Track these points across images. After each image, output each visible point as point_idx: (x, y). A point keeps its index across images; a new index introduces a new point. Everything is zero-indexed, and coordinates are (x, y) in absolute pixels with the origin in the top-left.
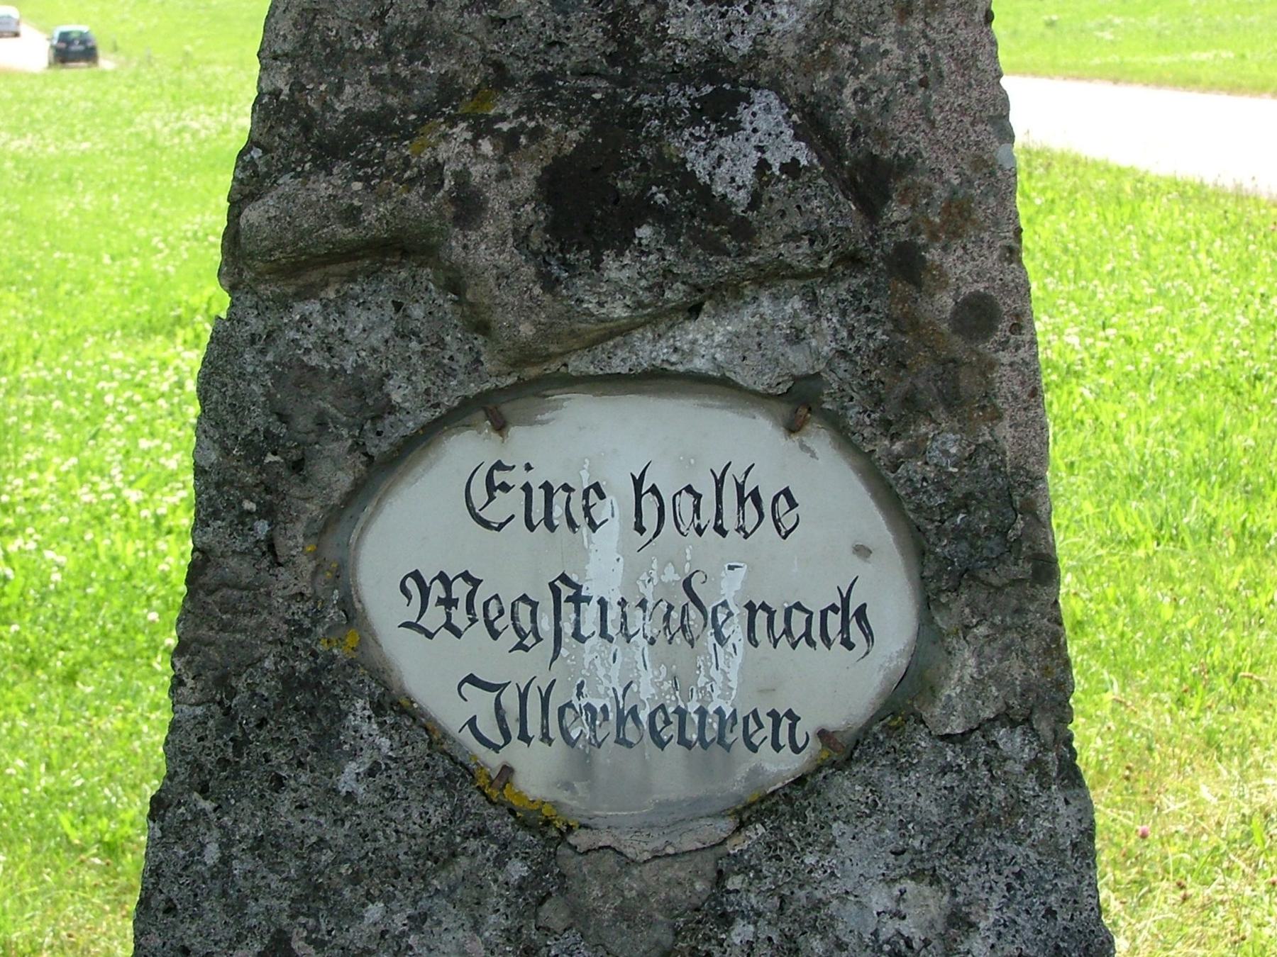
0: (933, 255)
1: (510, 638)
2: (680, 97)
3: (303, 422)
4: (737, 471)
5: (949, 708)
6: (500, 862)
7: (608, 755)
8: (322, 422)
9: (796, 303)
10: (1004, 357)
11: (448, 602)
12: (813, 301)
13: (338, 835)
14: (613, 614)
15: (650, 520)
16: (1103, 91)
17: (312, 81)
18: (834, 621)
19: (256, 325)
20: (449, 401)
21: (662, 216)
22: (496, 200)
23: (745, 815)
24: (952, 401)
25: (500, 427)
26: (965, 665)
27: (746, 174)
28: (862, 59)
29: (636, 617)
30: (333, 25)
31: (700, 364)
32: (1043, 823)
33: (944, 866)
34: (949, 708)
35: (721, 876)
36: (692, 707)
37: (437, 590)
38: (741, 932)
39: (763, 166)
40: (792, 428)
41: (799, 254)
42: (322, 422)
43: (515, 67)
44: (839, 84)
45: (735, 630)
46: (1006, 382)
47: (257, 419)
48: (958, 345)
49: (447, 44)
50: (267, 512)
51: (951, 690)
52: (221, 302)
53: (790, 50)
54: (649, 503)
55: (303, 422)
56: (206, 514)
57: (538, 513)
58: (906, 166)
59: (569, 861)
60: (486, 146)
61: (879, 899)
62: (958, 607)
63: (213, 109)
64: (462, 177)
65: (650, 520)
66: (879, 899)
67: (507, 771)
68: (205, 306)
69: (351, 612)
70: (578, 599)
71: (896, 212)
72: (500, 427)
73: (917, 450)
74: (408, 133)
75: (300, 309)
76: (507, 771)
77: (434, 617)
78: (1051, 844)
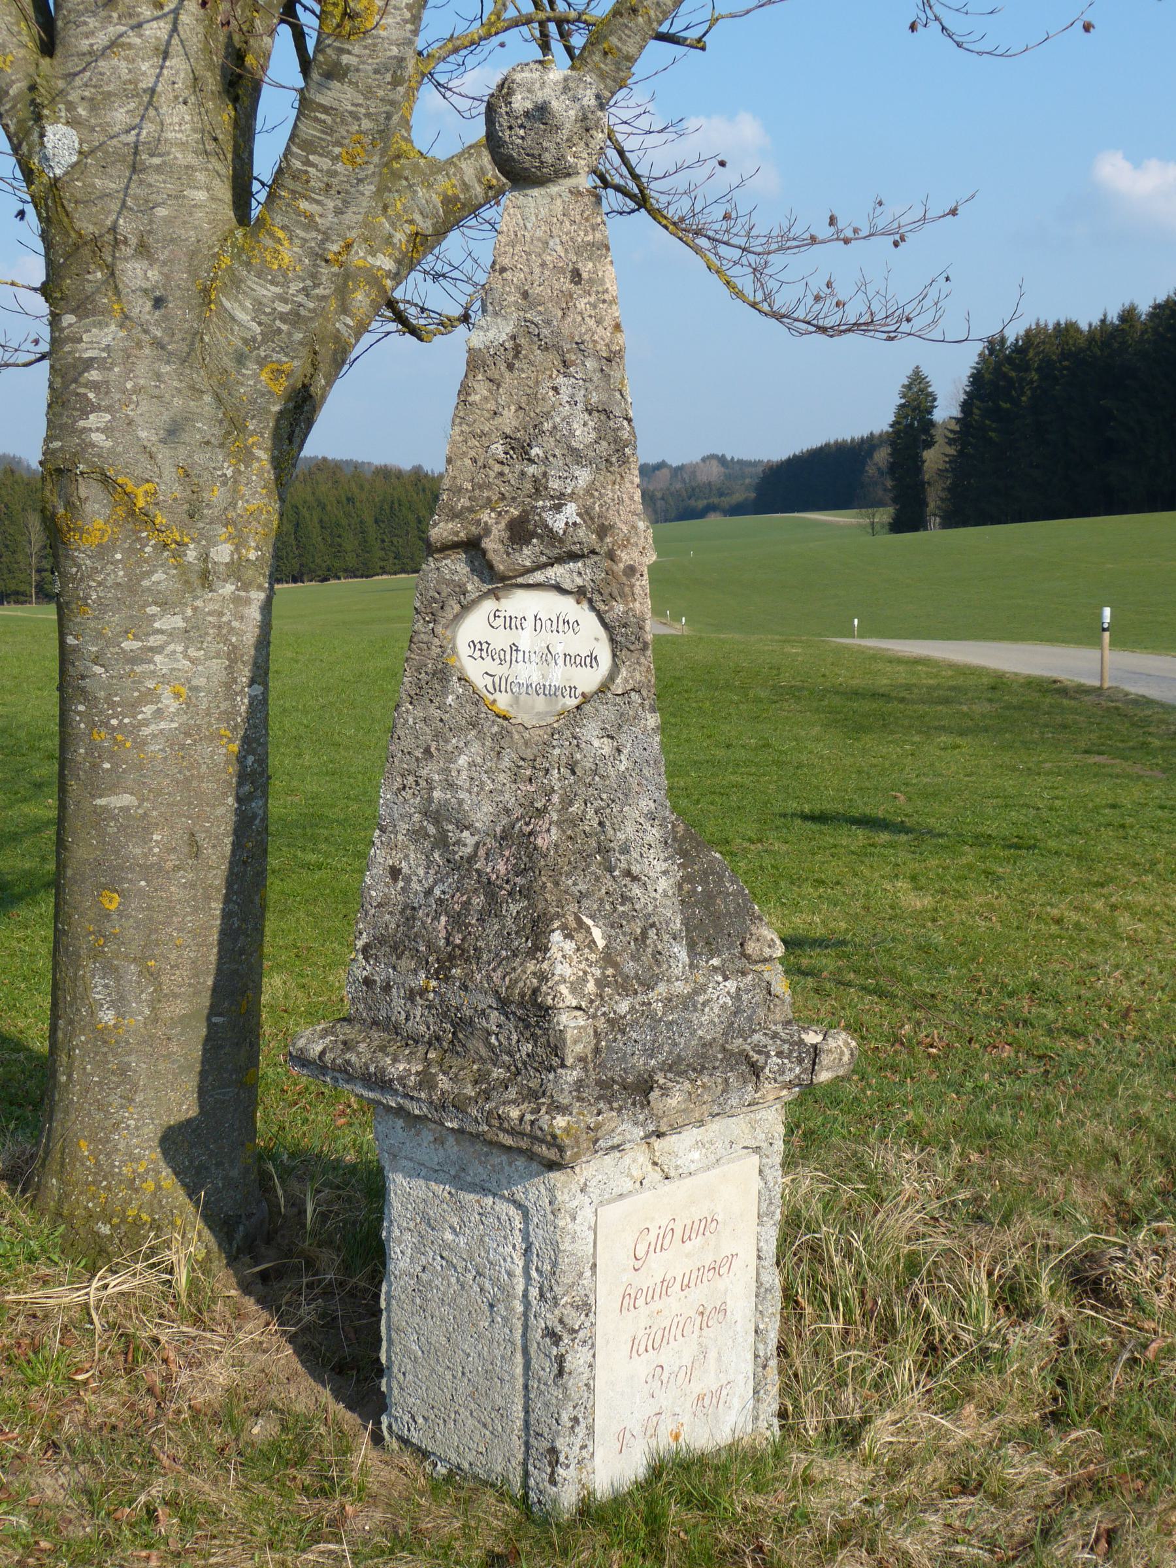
0: (618, 552)
4: (563, 614)
5: (618, 686)
7: (523, 697)
10: (638, 583)
11: (481, 650)
14: (527, 655)
15: (538, 628)
18: (588, 660)
21: (540, 537)
24: (623, 595)
26: (624, 672)
27: (563, 525)
29: (533, 655)
32: (643, 722)
34: (618, 686)
36: (547, 684)
37: (478, 646)
39: (567, 524)
43: (507, 494)
44: (594, 503)
45: (560, 661)
48: (624, 580)
53: (581, 492)
54: (538, 622)
57: (507, 625)
58: (612, 527)
60: (493, 515)
64: (486, 523)
65: (538, 628)
67: (494, 701)
70: (517, 650)
71: (608, 540)
72: (498, 599)
74: (475, 512)
75: (445, 562)
76: (494, 701)
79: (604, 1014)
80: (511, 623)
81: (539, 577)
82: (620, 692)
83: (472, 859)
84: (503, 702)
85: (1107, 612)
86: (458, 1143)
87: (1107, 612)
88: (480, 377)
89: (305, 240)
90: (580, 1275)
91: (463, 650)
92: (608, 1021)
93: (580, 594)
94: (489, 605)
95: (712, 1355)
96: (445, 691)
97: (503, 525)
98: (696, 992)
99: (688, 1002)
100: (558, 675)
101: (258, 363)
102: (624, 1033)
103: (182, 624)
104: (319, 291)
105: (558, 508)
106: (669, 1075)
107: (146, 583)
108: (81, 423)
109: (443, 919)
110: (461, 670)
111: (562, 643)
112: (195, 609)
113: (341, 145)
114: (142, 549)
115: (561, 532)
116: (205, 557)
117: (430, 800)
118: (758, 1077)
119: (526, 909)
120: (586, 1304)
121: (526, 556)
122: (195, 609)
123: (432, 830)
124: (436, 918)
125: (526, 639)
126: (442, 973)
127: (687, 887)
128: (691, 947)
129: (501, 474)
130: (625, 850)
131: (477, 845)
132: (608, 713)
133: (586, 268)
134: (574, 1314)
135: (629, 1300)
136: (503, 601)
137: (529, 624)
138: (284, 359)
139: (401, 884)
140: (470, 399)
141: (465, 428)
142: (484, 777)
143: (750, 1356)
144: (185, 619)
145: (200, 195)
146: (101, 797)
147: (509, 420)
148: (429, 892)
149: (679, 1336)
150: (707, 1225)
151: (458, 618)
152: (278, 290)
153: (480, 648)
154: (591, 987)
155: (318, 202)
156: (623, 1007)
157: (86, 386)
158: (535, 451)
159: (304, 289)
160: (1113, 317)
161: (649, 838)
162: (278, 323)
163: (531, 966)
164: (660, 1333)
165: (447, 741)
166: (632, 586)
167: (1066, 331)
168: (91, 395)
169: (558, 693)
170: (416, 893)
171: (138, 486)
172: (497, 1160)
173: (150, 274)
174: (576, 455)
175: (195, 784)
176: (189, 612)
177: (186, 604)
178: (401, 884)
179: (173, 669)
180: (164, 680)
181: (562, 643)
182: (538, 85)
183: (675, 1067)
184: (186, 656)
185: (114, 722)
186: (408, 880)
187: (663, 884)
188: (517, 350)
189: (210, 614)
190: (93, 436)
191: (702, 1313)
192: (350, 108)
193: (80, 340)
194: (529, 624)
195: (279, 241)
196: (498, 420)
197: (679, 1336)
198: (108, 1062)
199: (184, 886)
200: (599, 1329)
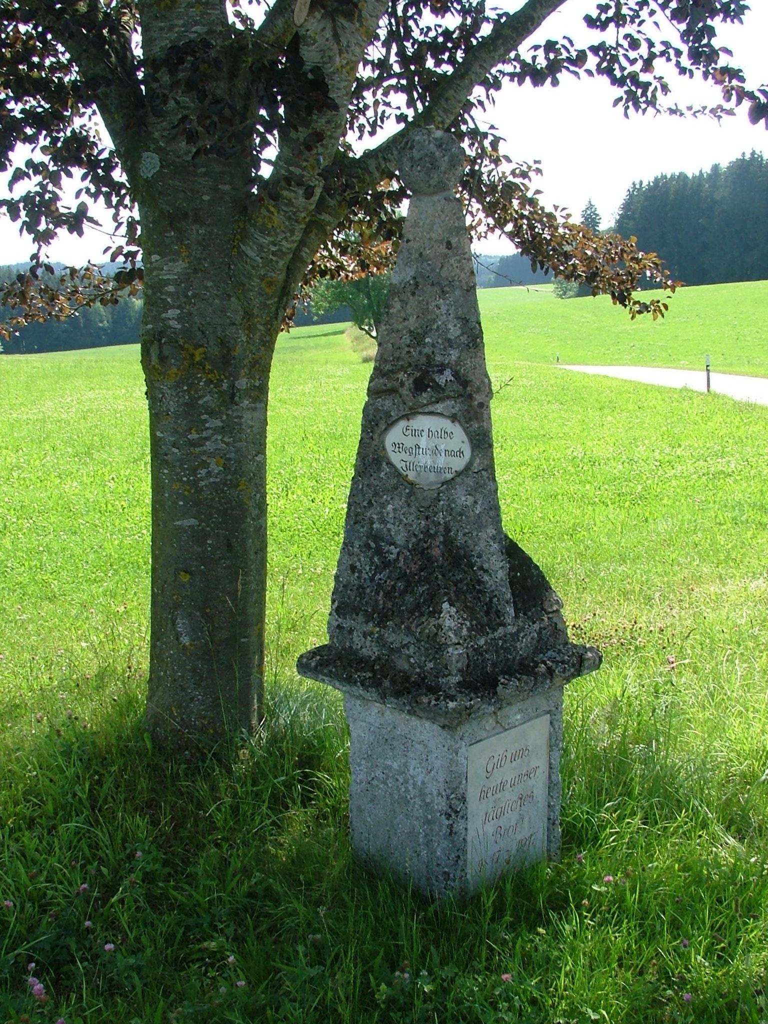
2: (436, 369)
3: (378, 417)
7: (423, 473)
8: (381, 418)
13: (380, 484)
16: (667, 370)
17: (206, 548)
19: (371, 402)
21: (431, 387)
22: (406, 384)
23: (443, 484)
24: (477, 419)
26: (478, 461)
28: (465, 365)
30: (386, 356)
33: (473, 493)
38: (442, 502)
40: (453, 422)
41: (452, 394)
42: (381, 418)
45: (443, 454)
46: (485, 416)
47: (371, 417)
49: (403, 359)
50: (372, 432)
51: (475, 465)
52: (367, 399)
55: (378, 417)
56: (363, 431)
58: (471, 381)
59: (415, 490)
61: (463, 499)
62: (477, 452)
63: (709, 822)
66: (463, 499)
69: (384, 448)
71: (469, 388)
73: (471, 426)
74: (396, 373)
77: (397, 450)
78: (490, 491)
79: (472, 646)
81: (431, 408)
83: (397, 560)
84: (411, 476)
86: (392, 714)
88: (396, 299)
89: (287, 212)
90: (460, 783)
91: (389, 447)
93: (454, 418)
94: (403, 424)
95: (526, 820)
96: (379, 470)
97: (411, 381)
98: (519, 631)
99: (515, 636)
100: (441, 461)
101: (260, 278)
102: (482, 655)
103: (220, 424)
105: (441, 372)
106: (506, 677)
107: (200, 402)
108: (164, 315)
109: (381, 593)
110: (388, 459)
112: (228, 415)
113: (307, 161)
114: (198, 384)
116: (232, 386)
117: (372, 529)
118: (552, 675)
119: (428, 589)
120: (463, 797)
121: (424, 397)
122: (228, 415)
123: (373, 545)
124: (378, 593)
125: (423, 442)
127: (512, 574)
128: (517, 611)
129: (409, 352)
130: (480, 556)
131: (398, 553)
132: (470, 482)
133: (454, 241)
134: (457, 803)
137: (425, 434)
139: (357, 574)
140: (391, 311)
141: (388, 327)
142: (402, 517)
143: (546, 819)
144: (222, 421)
145: (227, 188)
147: (412, 323)
148: (372, 579)
149: (509, 811)
150: (523, 752)
152: (271, 239)
153: (398, 446)
154: (465, 632)
156: (482, 642)
157: (166, 294)
159: (285, 238)
160: (707, 169)
161: (492, 550)
162: (271, 256)
163: (433, 622)
165: (381, 497)
166: (482, 413)
167: (682, 177)
168: (169, 300)
170: (365, 579)
171: (196, 349)
172: (414, 723)
173: (200, 231)
175: (229, 512)
176: (224, 417)
177: (223, 413)
178: (357, 574)
179: (217, 449)
180: (211, 455)
183: (509, 672)
185: (185, 479)
186: (360, 572)
187: (501, 574)
188: (417, 285)
193: (162, 269)
194: (425, 434)
195: (272, 213)
196: (406, 323)
197: (509, 811)
199: (225, 568)
200: (469, 811)
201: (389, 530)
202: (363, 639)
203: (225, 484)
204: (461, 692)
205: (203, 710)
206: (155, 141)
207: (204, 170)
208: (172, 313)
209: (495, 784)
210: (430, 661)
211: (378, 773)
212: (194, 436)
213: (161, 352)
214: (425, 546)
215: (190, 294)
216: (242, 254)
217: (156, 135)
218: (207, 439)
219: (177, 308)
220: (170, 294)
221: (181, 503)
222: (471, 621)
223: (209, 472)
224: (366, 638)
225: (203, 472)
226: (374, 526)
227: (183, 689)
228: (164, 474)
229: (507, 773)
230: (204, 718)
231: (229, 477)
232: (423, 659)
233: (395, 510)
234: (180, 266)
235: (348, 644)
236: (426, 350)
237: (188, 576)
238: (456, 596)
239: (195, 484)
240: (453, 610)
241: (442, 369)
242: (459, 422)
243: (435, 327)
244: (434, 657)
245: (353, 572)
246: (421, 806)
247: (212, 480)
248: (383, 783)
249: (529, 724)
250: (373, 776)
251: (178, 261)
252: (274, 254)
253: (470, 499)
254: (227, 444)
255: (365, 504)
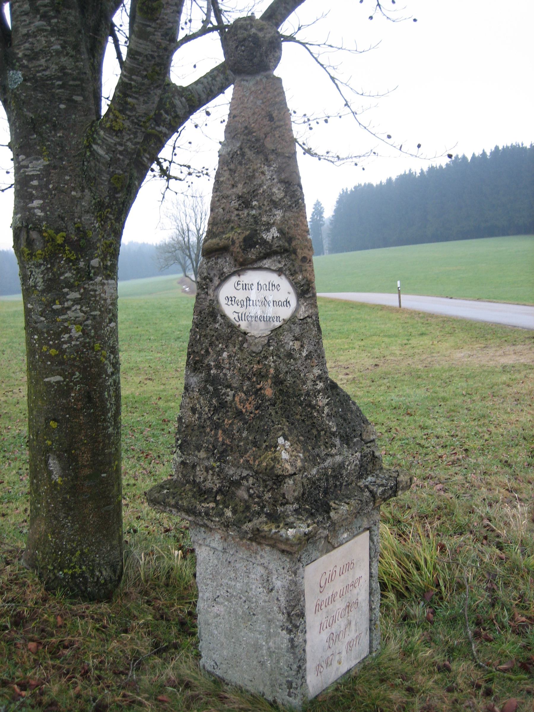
1: (240, 306)
3: (212, 275)
6: (238, 337)
7: (254, 322)
9: (279, 257)
11: (232, 301)
12: (281, 257)
20: (232, 271)
22: (237, 241)
25: (239, 275)
31: (266, 266)
35: (269, 340)
39: (273, 237)
40: (279, 275)
42: (215, 275)
45: (271, 304)
51: (301, 312)
61: (291, 343)
64: (233, 239)
68: (373, 564)
69: (218, 302)
72: (239, 275)
76: (239, 325)
77: (230, 303)
79: (306, 476)
80: (245, 287)
81: (260, 264)
82: (302, 318)
84: (243, 325)
85: (399, 282)
87: (399, 282)
92: (308, 479)
93: (280, 272)
94: (234, 279)
95: (353, 623)
96: (215, 321)
100: (270, 311)
103: (79, 296)
104: (137, 140)
105: (268, 230)
106: (337, 502)
107: (62, 278)
108: (30, 205)
111: (271, 296)
112: (85, 289)
115: (270, 241)
117: (209, 374)
122: (85, 289)
123: (211, 388)
125: (253, 295)
126: (221, 458)
135: (318, 607)
136: (241, 276)
137: (255, 287)
138: (121, 172)
139: (197, 415)
142: (236, 362)
146: (47, 377)
151: (220, 285)
152: (118, 140)
153: (231, 300)
155: (136, 98)
156: (314, 471)
158: (254, 203)
160: (384, 181)
162: (118, 155)
164: (332, 619)
165: (218, 346)
167: (370, 186)
168: (34, 192)
169: (271, 320)
171: (57, 233)
174: (275, 204)
176: (82, 291)
178: (197, 415)
179: (77, 317)
181: (271, 296)
182: (249, 27)
184: (82, 311)
185: (51, 343)
186: (200, 414)
189: (91, 291)
190: (36, 211)
191: (348, 606)
192: (151, 53)
194: (255, 287)
198: (57, 498)
201: (225, 375)
202: (205, 474)
203: (84, 346)
204: (299, 519)
205: (72, 535)
206: (19, 60)
207: (60, 83)
208: (36, 203)
209: (327, 597)
210: (268, 491)
211: (223, 592)
212: (57, 306)
213: (28, 236)
214: (258, 386)
215: (51, 186)
216: (93, 153)
217: (20, 55)
218: (69, 308)
219: (40, 199)
220: (35, 187)
221: (49, 363)
222: (304, 453)
223: (70, 337)
224: (207, 472)
225: (66, 336)
226: (212, 372)
227: (56, 518)
228: (35, 339)
229: (337, 586)
230: (73, 541)
231: (88, 340)
232: (261, 489)
233: (230, 356)
234: (42, 163)
235: (192, 478)
236: (254, 212)
237: (56, 423)
238: (290, 430)
239: (58, 347)
240: (288, 444)
241: (268, 226)
242: (285, 275)
243: (261, 191)
244: (272, 488)
245: (194, 413)
246: (263, 622)
247: (73, 343)
248: (228, 600)
249: (352, 541)
250: (218, 594)
251: (40, 159)
252: (121, 153)
253: (297, 345)
254: (85, 313)
255: (203, 352)
